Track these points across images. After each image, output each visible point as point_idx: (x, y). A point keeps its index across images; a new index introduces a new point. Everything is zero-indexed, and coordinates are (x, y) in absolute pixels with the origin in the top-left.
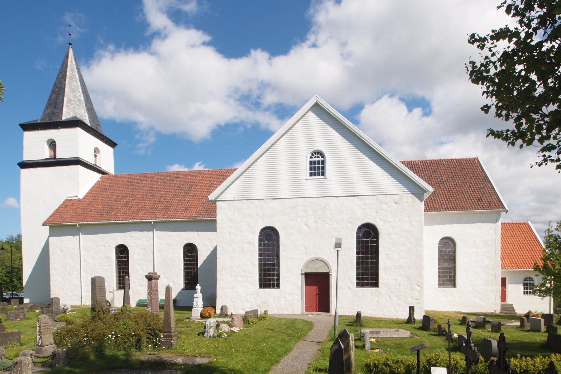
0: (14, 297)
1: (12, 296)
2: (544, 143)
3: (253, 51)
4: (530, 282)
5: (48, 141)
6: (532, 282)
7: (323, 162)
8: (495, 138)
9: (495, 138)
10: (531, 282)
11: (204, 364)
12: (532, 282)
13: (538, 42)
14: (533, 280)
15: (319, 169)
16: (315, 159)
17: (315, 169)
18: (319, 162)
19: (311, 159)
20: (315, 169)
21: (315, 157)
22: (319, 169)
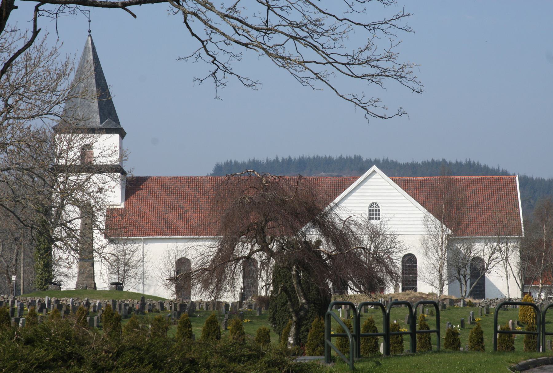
0: (417, 335)
1: (418, 332)
2: (434, 314)
3: (421, 163)
4: (373, 208)
5: (373, 204)
6: (378, 208)
7: (379, 210)
8: (290, 158)
9: (290, 158)
10: (377, 208)
11: (283, 160)
12: (378, 208)
13: (3, 30)
14: (379, 207)
15: (373, 214)
16: (373, 208)
17: (376, 214)
18: (376, 210)
19: (370, 208)
20: (376, 214)
21: (373, 207)
22: (373, 214)
